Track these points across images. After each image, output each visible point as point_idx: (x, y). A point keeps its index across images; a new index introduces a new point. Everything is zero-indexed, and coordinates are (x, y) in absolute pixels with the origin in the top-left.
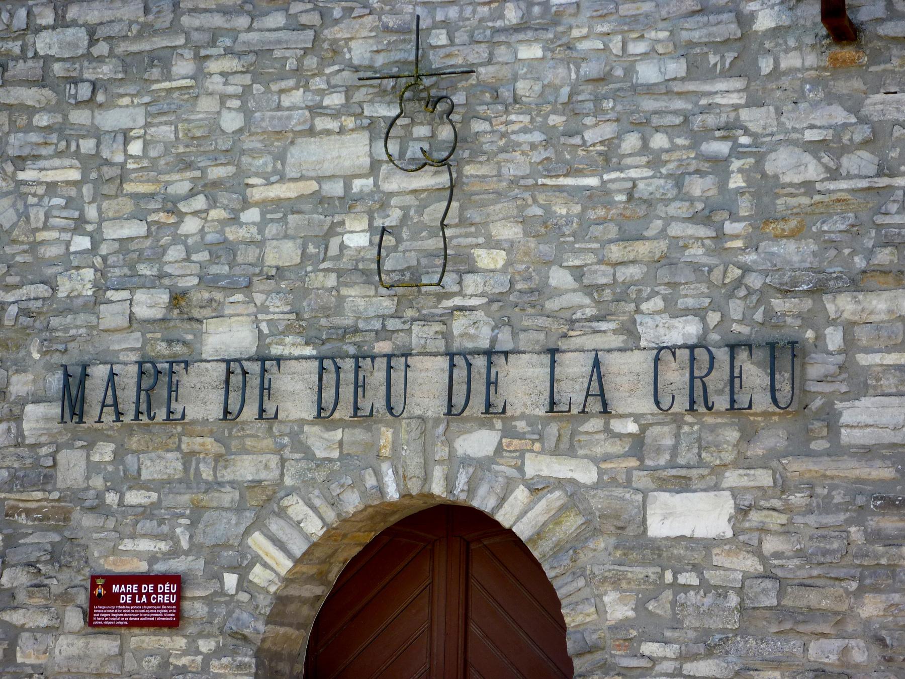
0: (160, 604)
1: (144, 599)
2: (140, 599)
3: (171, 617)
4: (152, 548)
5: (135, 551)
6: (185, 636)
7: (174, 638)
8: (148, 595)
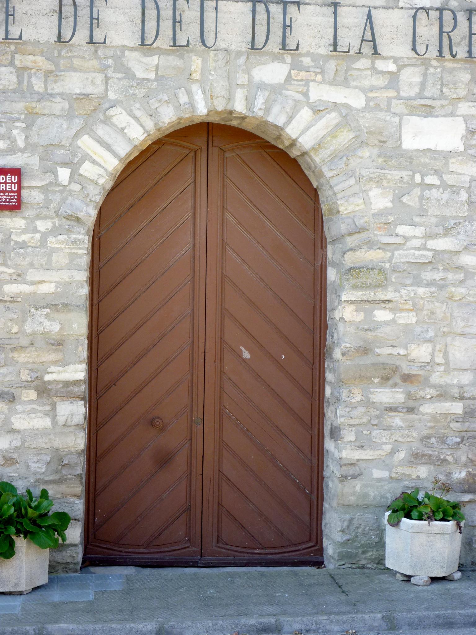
3: (14, 202)
6: (24, 218)
7: (14, 219)
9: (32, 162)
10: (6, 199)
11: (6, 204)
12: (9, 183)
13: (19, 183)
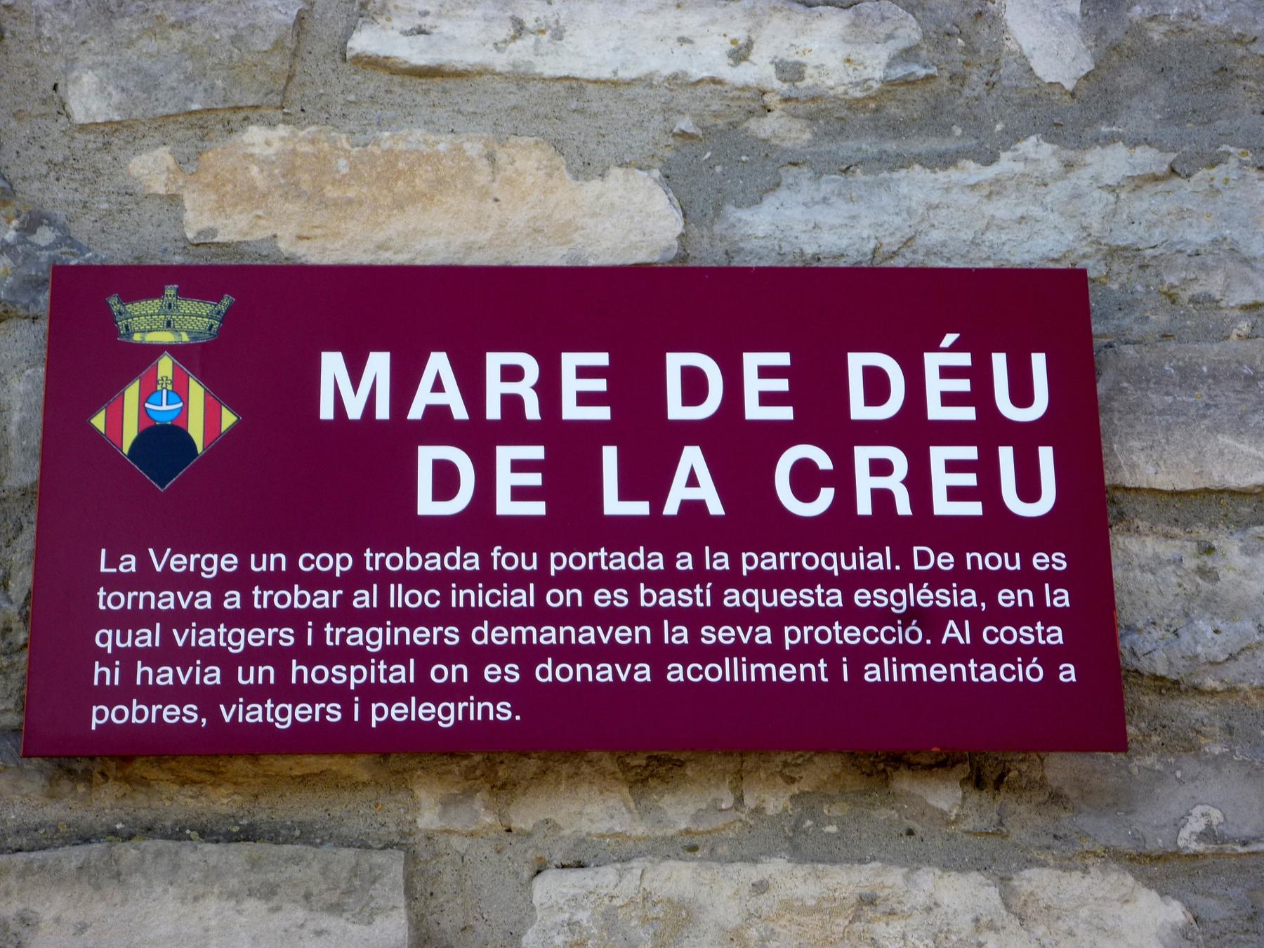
0: (884, 526)
1: (694, 481)
2: (647, 477)
3: (1026, 653)
4: (709, 59)
5: (521, 78)
6: (1157, 866)
7: (1039, 882)
8: (740, 450)
9: (1197, 236)
10: (932, 619)
11: (937, 673)
12: (951, 433)
13: (1076, 428)
